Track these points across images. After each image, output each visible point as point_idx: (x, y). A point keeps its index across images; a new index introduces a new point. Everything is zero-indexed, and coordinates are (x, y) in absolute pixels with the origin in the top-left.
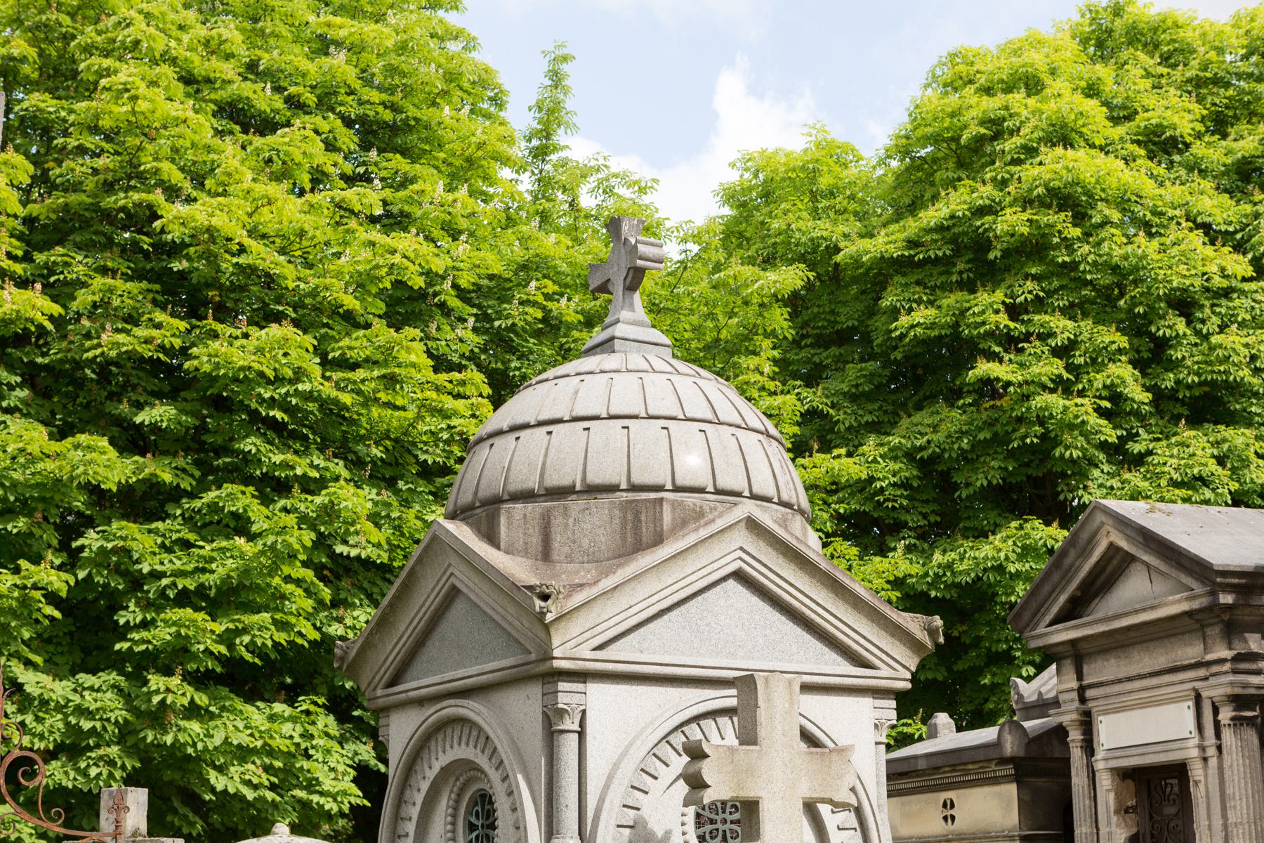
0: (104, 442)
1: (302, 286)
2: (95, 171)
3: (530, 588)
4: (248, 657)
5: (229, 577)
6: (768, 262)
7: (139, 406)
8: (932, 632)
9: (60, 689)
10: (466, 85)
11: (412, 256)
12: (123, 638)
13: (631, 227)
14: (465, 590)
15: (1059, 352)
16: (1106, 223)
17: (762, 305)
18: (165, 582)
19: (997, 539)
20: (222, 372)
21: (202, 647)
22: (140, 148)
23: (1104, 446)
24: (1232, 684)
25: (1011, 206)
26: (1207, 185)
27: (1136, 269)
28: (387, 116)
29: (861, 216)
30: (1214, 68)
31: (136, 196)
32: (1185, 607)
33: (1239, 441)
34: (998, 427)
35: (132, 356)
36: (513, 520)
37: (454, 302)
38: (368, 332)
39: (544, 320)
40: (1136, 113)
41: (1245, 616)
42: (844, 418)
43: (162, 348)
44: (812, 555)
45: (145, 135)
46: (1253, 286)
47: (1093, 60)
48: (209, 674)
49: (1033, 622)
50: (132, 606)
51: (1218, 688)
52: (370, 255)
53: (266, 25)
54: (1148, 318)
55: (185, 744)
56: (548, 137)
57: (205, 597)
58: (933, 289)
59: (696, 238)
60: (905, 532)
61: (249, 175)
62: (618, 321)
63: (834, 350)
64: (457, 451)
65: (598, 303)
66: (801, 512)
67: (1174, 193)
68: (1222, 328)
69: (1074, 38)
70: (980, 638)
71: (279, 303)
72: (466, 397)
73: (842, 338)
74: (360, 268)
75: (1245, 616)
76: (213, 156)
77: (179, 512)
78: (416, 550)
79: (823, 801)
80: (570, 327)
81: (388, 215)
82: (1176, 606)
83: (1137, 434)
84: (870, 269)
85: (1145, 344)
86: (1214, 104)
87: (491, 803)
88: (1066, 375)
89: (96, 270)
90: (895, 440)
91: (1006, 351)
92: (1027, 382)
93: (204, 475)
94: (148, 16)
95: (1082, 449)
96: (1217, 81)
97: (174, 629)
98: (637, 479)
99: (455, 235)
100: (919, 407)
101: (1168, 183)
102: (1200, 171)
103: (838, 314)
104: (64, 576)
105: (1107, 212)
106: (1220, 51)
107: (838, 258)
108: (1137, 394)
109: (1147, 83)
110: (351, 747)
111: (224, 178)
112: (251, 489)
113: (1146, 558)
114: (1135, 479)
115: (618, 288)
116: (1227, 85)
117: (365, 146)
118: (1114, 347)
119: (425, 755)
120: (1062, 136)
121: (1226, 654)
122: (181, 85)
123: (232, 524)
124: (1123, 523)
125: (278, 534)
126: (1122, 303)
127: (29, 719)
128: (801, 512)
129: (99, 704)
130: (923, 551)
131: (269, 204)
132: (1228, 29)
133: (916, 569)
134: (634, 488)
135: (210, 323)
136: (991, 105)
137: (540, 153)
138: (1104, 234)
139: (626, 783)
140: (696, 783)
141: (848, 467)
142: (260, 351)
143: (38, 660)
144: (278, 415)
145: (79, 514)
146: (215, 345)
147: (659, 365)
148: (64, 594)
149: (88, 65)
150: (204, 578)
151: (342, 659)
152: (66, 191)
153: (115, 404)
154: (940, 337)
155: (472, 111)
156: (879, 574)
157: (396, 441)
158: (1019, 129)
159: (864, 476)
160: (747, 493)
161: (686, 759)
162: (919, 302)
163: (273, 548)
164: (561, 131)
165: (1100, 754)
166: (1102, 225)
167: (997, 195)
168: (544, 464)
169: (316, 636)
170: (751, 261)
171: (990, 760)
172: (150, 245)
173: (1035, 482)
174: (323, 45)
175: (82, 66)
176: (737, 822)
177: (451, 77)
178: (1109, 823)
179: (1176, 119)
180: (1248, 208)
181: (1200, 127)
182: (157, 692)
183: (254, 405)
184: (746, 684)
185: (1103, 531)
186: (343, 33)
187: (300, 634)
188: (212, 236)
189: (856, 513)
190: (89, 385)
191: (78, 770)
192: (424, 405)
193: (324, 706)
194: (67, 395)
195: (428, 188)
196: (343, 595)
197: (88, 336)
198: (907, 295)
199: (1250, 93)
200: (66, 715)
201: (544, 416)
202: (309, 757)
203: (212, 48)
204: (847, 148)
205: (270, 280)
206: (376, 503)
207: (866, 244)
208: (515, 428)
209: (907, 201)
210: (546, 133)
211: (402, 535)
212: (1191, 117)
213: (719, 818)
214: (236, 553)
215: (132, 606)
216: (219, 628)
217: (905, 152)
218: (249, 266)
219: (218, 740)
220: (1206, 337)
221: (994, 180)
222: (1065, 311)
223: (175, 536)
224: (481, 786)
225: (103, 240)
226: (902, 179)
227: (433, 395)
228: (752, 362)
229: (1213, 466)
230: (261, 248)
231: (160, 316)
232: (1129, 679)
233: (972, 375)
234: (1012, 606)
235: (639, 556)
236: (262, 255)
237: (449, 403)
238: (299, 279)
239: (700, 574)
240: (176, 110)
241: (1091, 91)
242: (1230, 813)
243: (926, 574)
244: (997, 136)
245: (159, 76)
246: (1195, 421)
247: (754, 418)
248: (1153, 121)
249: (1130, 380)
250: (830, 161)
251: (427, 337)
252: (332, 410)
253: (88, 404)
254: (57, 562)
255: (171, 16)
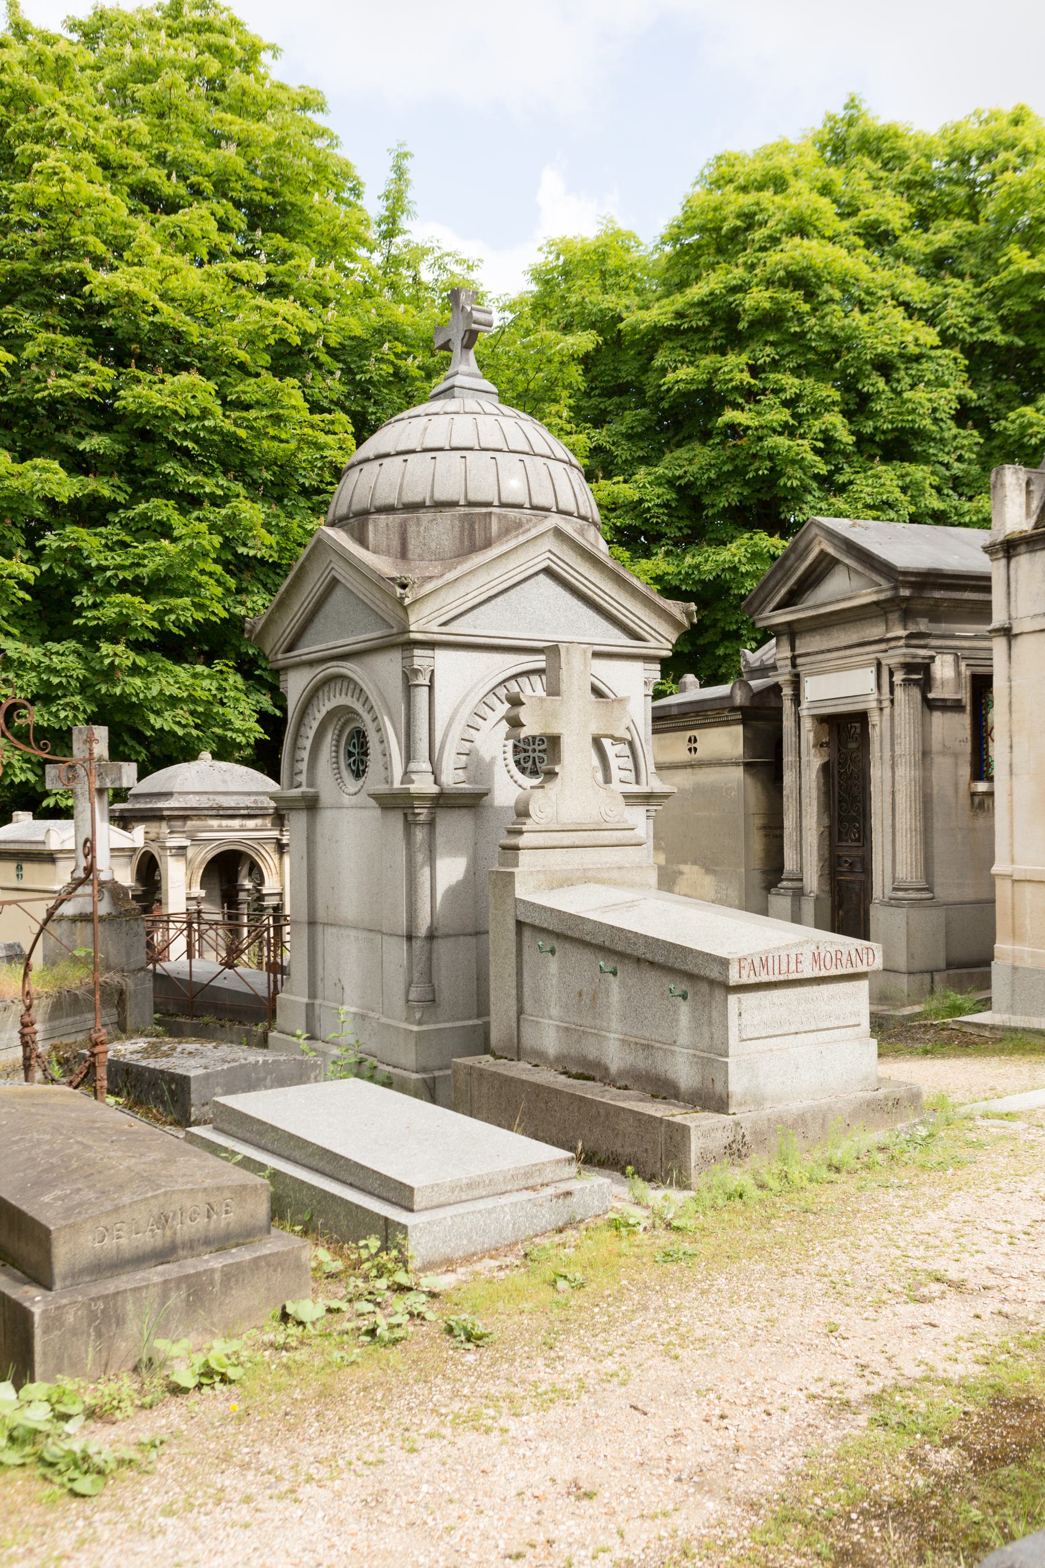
0: (55, 465)
1: (205, 341)
2: (35, 243)
3: (393, 579)
4: (175, 630)
5: (158, 570)
6: (567, 328)
7: (81, 437)
8: (689, 615)
9: (33, 654)
10: (332, 177)
11: (291, 318)
12: (79, 616)
13: (467, 296)
14: (343, 581)
15: (787, 404)
16: (831, 300)
17: (562, 363)
18: (109, 573)
19: (733, 547)
20: (144, 410)
21: (139, 623)
22: (69, 224)
23: (816, 477)
24: (904, 655)
25: (757, 285)
26: (910, 270)
27: (849, 338)
28: (270, 200)
29: (639, 292)
30: (923, 173)
31: (68, 265)
32: (874, 598)
33: (919, 475)
34: (738, 462)
35: (72, 396)
36: (379, 527)
37: (324, 358)
38: (258, 380)
39: (396, 374)
40: (859, 210)
41: (917, 605)
42: (622, 452)
43: (96, 390)
44: (602, 557)
45: (73, 213)
46: (939, 352)
47: (829, 164)
48: (146, 642)
49: (760, 608)
50: (85, 592)
51: (894, 657)
52: (258, 317)
53: (171, 120)
54: (856, 378)
55: (131, 694)
56: (393, 224)
57: (141, 585)
58: (694, 352)
59: (511, 308)
60: (664, 541)
61: (158, 248)
62: (457, 373)
63: (616, 399)
64: (328, 478)
65: (436, 359)
66: (595, 524)
67: (884, 276)
68: (913, 386)
69: (814, 144)
70: (717, 621)
71: (188, 356)
72: (335, 433)
73: (622, 389)
74: (250, 327)
75: (917, 605)
76: (129, 232)
77: (117, 520)
78: (303, 553)
79: (606, 736)
80: (415, 379)
81: (269, 285)
82: (868, 596)
83: (842, 468)
84: (645, 335)
85: (853, 400)
86: (920, 203)
87: (364, 737)
88: (791, 422)
89: (40, 325)
90: (660, 470)
91: (747, 402)
92: (762, 427)
93: (135, 491)
94: (69, 107)
95: (801, 480)
96: (925, 184)
97: (117, 609)
98: (472, 497)
99: (325, 302)
100: (679, 445)
101: (879, 269)
102: (905, 259)
103: (620, 371)
104: (32, 568)
105: (831, 291)
106: (929, 158)
107: (621, 326)
108: (845, 437)
109: (868, 184)
110: (255, 696)
111: (137, 250)
112: (172, 502)
113: (847, 561)
114: (839, 503)
115: (457, 346)
116: (932, 188)
117: (252, 227)
118: (829, 400)
119: (315, 702)
120: (800, 228)
121: (902, 633)
122: (100, 170)
123: (159, 530)
124: (832, 535)
125: (194, 538)
126: (837, 365)
127: (11, 676)
128: (595, 524)
129: (64, 665)
130: (678, 555)
131: (176, 273)
132: (937, 139)
133: (671, 569)
134: (471, 504)
135: (133, 370)
136: (746, 201)
137: (389, 235)
138: (827, 309)
139: (464, 723)
140: (515, 723)
141: (625, 491)
142: (173, 394)
143: (16, 632)
144: (190, 444)
145: (39, 521)
146: (138, 389)
147: (489, 408)
148: (32, 582)
149: (24, 149)
150: (139, 571)
151: (251, 632)
152: (11, 258)
153: (62, 434)
154: (698, 390)
155: (336, 199)
156: (645, 572)
157: (281, 467)
158: (766, 222)
159: (636, 498)
160: (554, 509)
161: (508, 706)
162: (682, 362)
163: (191, 546)
164: (404, 217)
165: (804, 705)
166: (826, 302)
167: (747, 276)
168: (401, 485)
169: (224, 614)
170: (553, 327)
171: (724, 709)
172: (83, 305)
173: (763, 504)
174: (216, 140)
175: (17, 151)
176: (544, 751)
177: (319, 168)
178: (808, 754)
179: (889, 216)
180: (939, 289)
181: (907, 223)
182: (107, 656)
183: (171, 437)
184: (552, 651)
185: (816, 541)
186: (235, 128)
187: (213, 613)
188: (131, 299)
189: (629, 527)
190: (41, 419)
191: (50, 713)
192: (303, 440)
193: (233, 667)
194: (24, 427)
195: (304, 264)
196: (244, 585)
197: (37, 380)
198: (674, 357)
199: (949, 195)
200: (39, 674)
201: (401, 447)
202: (223, 704)
203: (126, 138)
204: (631, 236)
205: (178, 337)
206: (268, 515)
207: (643, 314)
208: (360, 462)
209: (677, 280)
210: (392, 219)
211: (288, 539)
212: (901, 214)
213: (530, 748)
214: (162, 552)
215: (85, 592)
216: (151, 608)
217: (675, 239)
218: (162, 324)
219: (155, 692)
220: (899, 394)
221: (745, 263)
222: (796, 372)
223: (115, 538)
224: (357, 725)
225: (44, 300)
226: (673, 262)
227: (309, 431)
228: (554, 408)
229: (898, 494)
230: (171, 310)
231: (94, 365)
232: (829, 651)
233: (721, 421)
234: (742, 597)
235: (473, 556)
236: (169, 314)
237: (322, 438)
238: (202, 336)
239: (519, 570)
240: (96, 191)
241: (825, 190)
242: (897, 748)
243: (680, 573)
244: (749, 228)
245: (81, 161)
246: (887, 458)
247: (561, 452)
248: (872, 217)
249: (839, 426)
250: (617, 247)
251: (304, 385)
252: (231, 441)
253: (41, 434)
254: (25, 557)
255: (88, 108)
